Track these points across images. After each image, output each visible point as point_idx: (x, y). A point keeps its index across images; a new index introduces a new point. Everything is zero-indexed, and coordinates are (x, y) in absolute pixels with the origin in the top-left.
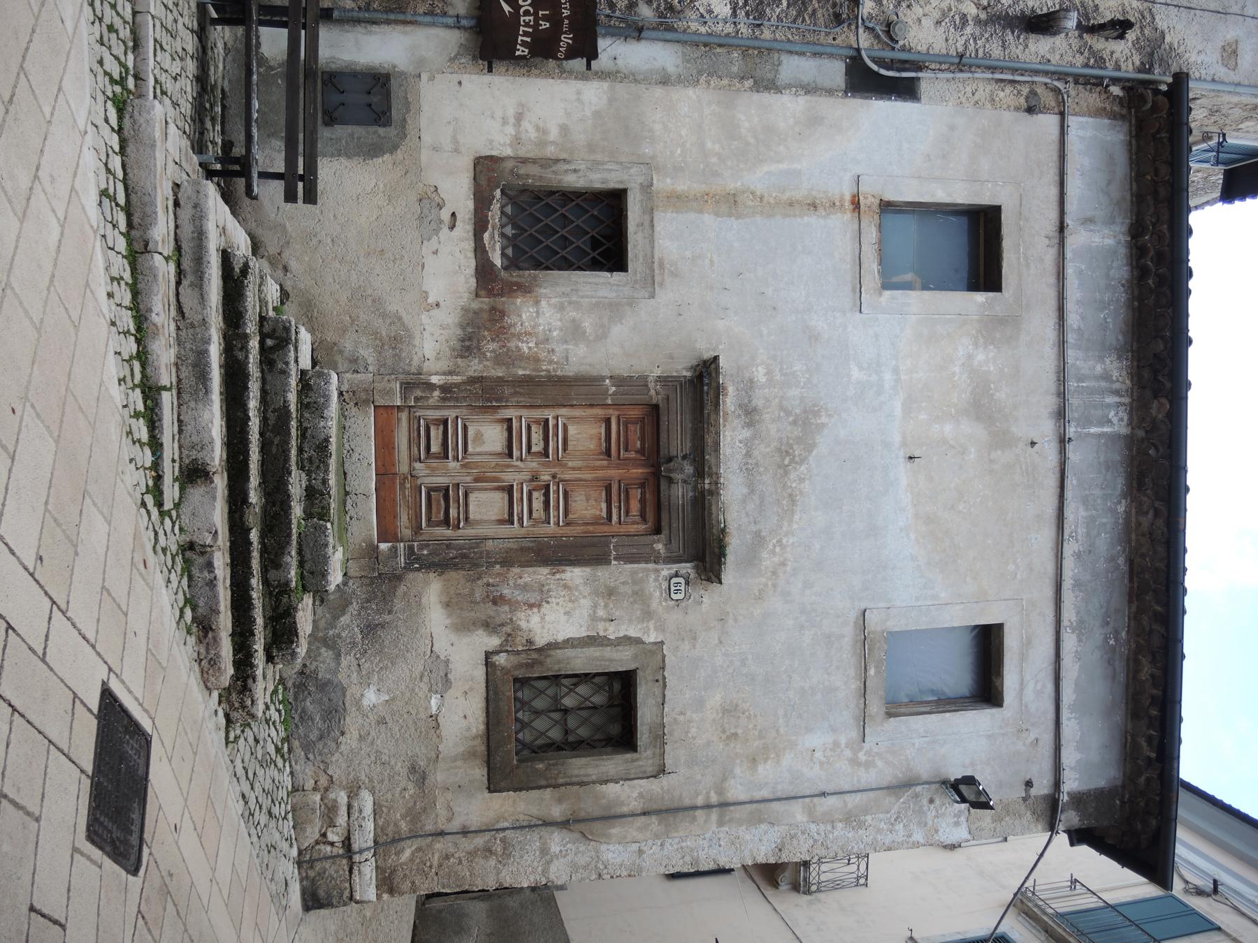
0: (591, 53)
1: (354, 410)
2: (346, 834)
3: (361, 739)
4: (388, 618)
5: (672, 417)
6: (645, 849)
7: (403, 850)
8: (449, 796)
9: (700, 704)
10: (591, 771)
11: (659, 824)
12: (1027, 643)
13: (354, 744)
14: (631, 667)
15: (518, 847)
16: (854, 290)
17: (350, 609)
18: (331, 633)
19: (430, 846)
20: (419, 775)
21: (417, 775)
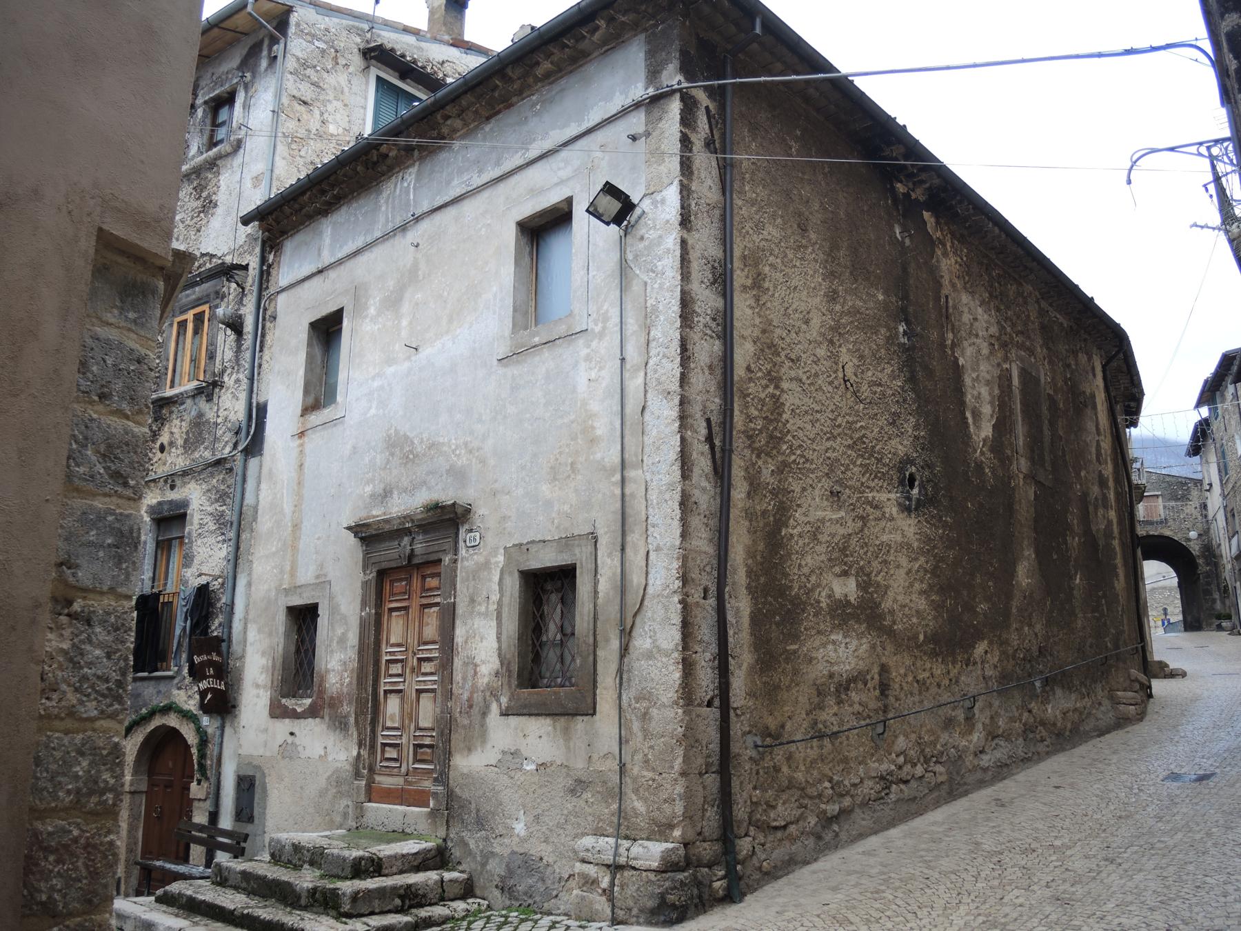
0: (219, 640)
1: (365, 819)
2: (604, 869)
3: (546, 841)
4: (473, 806)
5: (383, 559)
6: (655, 544)
7: (633, 809)
8: (595, 757)
9: (548, 504)
10: (586, 610)
11: (634, 532)
12: (534, 192)
13: (550, 849)
14: (516, 575)
15: (644, 684)
16: (335, 425)
17: (466, 838)
18: (479, 859)
19: (635, 780)
20: (578, 786)
21: (578, 788)
